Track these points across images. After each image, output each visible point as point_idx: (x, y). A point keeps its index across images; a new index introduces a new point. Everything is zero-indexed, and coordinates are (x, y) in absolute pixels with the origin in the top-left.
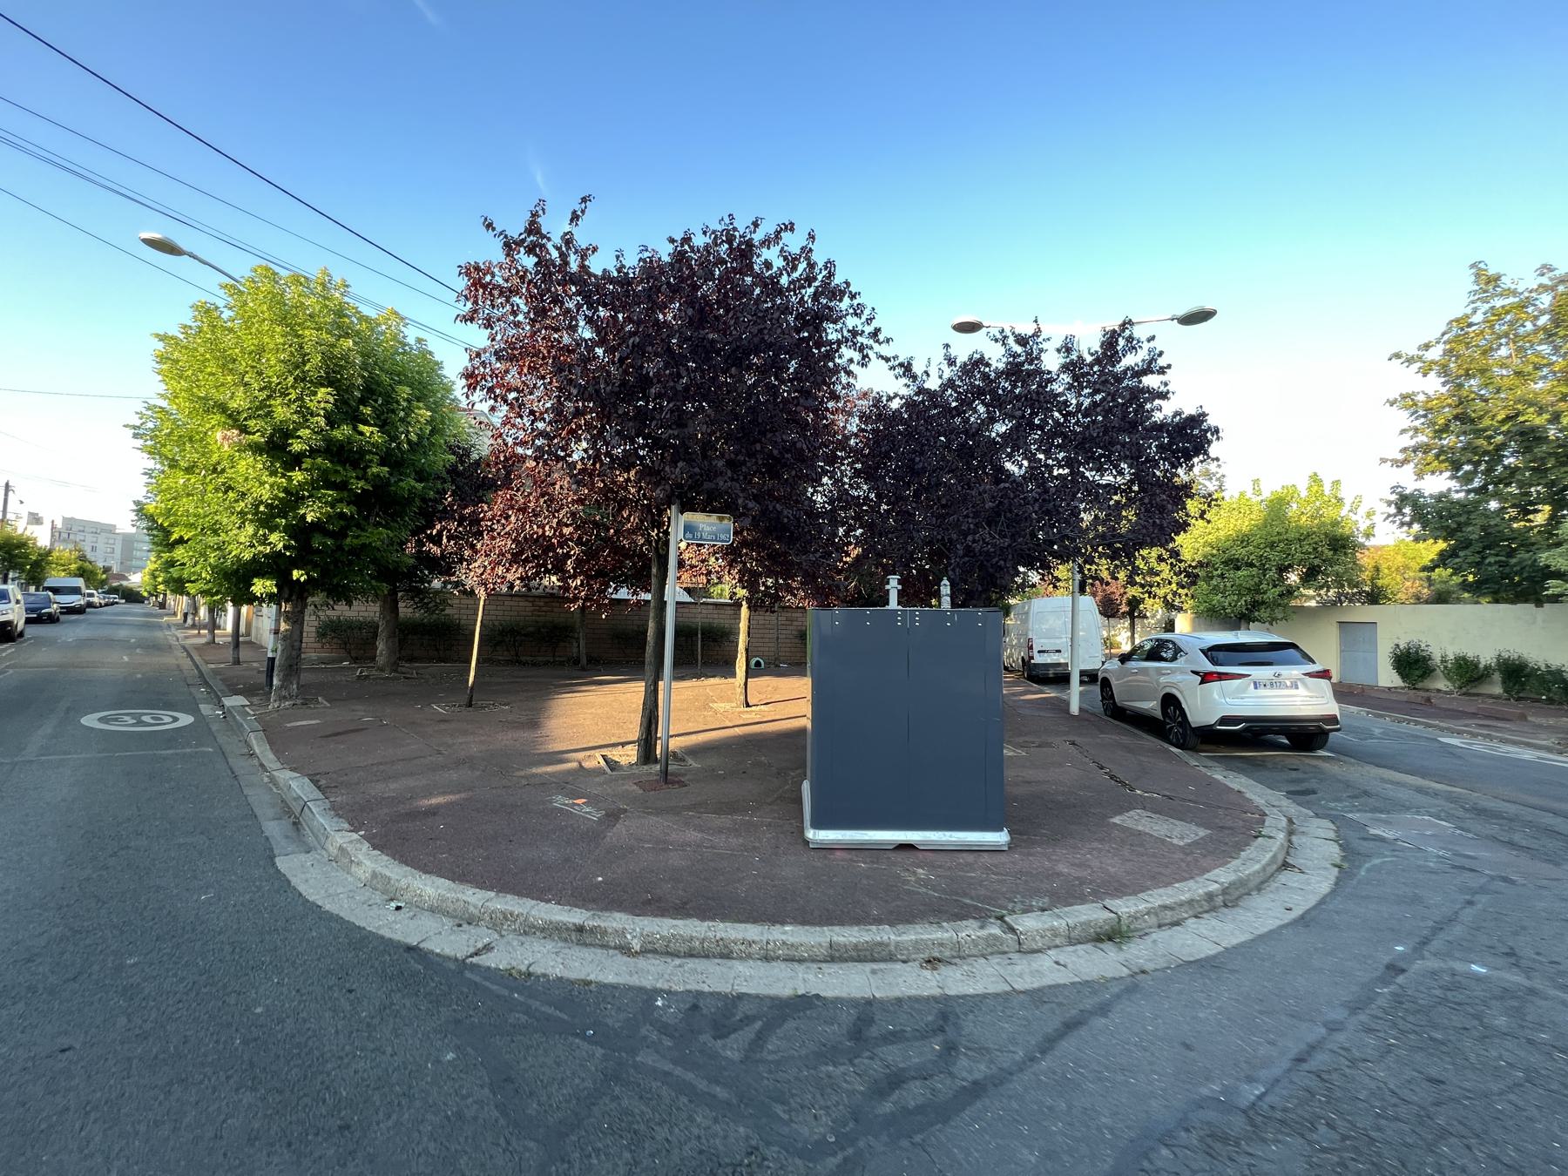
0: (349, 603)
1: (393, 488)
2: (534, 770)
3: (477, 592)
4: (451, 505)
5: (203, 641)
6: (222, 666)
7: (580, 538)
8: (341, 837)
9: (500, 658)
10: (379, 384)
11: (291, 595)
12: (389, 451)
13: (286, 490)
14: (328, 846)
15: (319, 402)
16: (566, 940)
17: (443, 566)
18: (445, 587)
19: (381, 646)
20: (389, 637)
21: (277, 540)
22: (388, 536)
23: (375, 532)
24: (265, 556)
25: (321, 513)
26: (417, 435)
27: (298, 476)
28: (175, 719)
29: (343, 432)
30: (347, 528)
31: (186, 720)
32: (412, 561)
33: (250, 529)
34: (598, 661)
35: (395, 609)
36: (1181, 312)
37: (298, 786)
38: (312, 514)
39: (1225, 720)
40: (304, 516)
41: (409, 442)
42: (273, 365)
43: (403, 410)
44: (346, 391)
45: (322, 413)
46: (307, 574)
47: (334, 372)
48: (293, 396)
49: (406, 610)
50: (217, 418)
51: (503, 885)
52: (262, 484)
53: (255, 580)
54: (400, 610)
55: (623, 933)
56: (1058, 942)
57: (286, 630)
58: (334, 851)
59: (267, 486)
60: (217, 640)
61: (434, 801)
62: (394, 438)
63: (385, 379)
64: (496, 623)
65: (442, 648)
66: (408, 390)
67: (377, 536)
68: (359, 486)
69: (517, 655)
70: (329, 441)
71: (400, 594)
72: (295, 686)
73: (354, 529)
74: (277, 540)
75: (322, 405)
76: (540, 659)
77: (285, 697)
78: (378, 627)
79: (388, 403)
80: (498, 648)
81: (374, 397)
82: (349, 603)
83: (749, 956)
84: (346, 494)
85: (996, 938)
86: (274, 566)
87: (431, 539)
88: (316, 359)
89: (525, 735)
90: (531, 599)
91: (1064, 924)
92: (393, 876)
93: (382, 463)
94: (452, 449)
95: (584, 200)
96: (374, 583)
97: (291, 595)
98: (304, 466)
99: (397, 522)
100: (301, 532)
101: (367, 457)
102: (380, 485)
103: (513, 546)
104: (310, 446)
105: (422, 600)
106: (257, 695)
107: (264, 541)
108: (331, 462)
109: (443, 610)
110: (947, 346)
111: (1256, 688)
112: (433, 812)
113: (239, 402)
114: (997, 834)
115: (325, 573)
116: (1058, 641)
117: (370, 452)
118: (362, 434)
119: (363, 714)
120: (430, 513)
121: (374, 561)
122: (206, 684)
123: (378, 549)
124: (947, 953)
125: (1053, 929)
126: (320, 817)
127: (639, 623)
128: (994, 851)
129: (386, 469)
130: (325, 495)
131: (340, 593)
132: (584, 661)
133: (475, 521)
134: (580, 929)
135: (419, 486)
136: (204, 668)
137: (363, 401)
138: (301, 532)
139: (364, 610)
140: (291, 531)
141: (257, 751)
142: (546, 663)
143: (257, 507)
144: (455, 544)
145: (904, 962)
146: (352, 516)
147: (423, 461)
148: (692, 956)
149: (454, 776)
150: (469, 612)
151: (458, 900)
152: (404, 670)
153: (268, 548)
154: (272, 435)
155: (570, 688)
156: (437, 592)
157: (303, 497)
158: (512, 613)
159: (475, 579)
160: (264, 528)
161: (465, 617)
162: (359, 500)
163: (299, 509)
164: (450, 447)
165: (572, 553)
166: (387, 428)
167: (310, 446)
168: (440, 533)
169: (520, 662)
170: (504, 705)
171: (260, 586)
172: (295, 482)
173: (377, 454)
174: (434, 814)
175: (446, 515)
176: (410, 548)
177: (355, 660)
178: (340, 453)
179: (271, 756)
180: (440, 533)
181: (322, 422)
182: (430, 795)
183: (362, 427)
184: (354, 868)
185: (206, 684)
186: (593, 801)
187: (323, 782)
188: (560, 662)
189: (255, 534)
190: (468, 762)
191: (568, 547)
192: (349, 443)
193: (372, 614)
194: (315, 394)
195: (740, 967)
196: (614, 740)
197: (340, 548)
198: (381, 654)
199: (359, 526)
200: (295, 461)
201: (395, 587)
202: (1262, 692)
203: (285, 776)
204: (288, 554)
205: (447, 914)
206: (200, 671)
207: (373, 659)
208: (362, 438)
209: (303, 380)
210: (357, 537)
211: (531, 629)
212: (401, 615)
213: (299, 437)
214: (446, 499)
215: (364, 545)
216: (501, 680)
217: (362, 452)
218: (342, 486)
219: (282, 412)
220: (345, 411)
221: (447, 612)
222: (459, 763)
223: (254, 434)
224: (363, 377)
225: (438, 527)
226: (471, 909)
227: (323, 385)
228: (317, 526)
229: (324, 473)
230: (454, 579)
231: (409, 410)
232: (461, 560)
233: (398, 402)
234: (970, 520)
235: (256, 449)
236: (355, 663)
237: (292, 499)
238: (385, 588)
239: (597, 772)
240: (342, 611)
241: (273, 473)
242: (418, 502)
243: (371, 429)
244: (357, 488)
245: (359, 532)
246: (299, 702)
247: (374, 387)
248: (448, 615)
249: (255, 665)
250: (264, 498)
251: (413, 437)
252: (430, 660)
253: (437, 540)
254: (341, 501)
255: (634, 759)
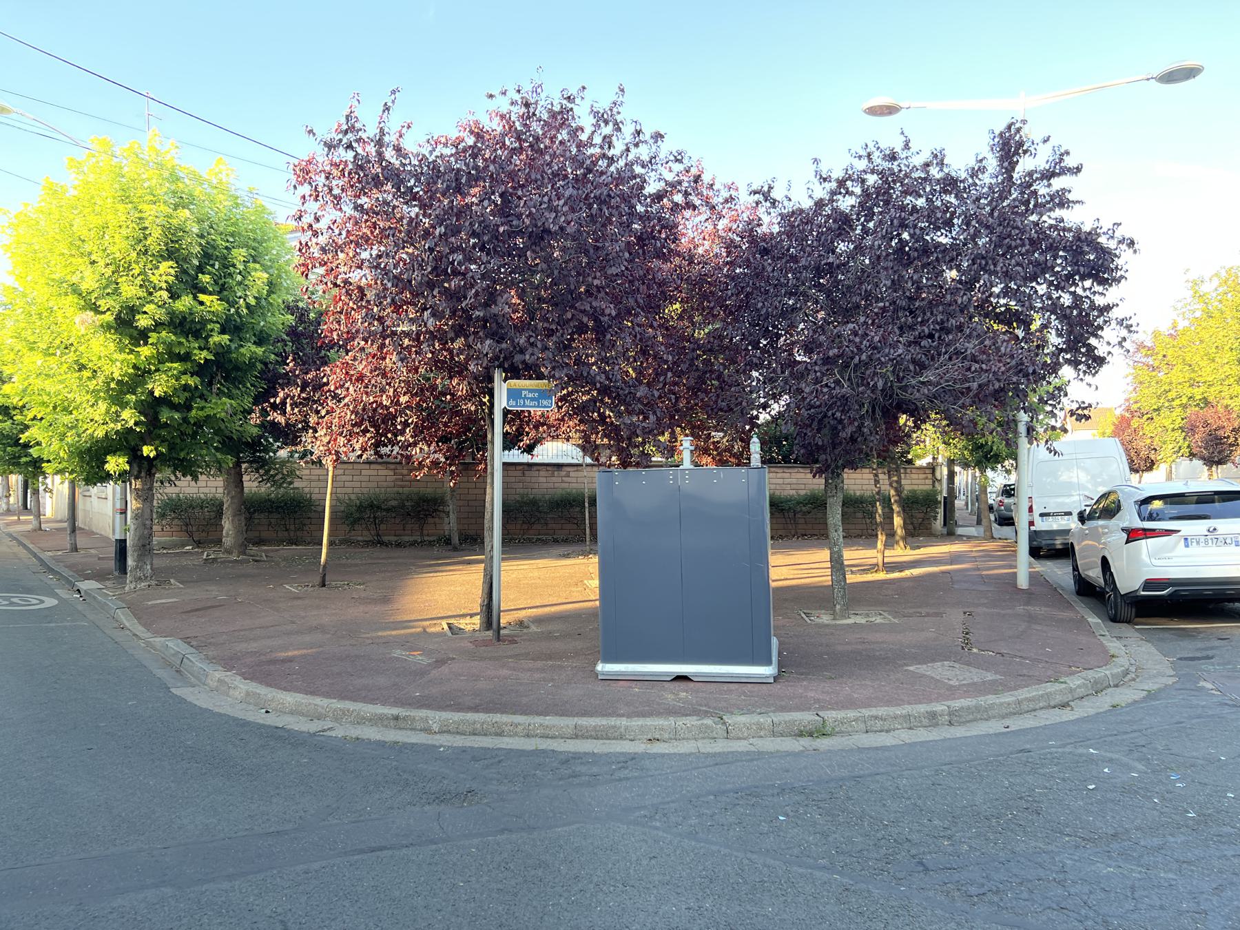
0: (195, 478)
1: (234, 355)
2: (380, 634)
3: (324, 462)
4: (293, 371)
5: (30, 527)
6: (60, 553)
7: (418, 404)
8: (217, 674)
9: (360, 538)
10: (214, 248)
11: (140, 472)
12: (229, 319)
13: (135, 367)
14: (209, 681)
15: (161, 275)
16: (386, 726)
17: (289, 435)
18: (292, 456)
19: (227, 524)
20: (234, 516)
21: (129, 417)
22: (231, 405)
23: (219, 402)
24: (117, 432)
25: (167, 387)
26: (256, 298)
27: (146, 351)
28: (42, 602)
29: (185, 303)
30: (192, 399)
31: (50, 602)
32: (255, 431)
33: (103, 406)
34: (476, 540)
35: (240, 483)
36: (1159, 69)
37: (175, 645)
38: (160, 388)
39: (1149, 584)
40: (151, 392)
41: (248, 306)
42: (119, 246)
43: (240, 273)
44: (185, 260)
45: (164, 285)
46: (156, 449)
47: (172, 241)
48: (136, 272)
49: (252, 484)
50: (72, 298)
51: (342, 696)
52: (113, 362)
53: (109, 458)
54: (246, 484)
55: (426, 720)
56: (762, 734)
57: (138, 509)
58: (214, 684)
59: (118, 364)
60: (43, 526)
61: (290, 654)
62: (232, 304)
63: (221, 243)
64: (353, 497)
65: (292, 527)
66: (243, 251)
67: (221, 406)
68: (202, 356)
69: (378, 535)
70: (172, 314)
71: (244, 466)
72: (149, 567)
73: (198, 400)
74: (129, 417)
75: (164, 278)
76: (406, 538)
77: (140, 578)
78: (222, 504)
79: (225, 266)
80: (356, 527)
81: (211, 262)
82: (195, 478)
83: (516, 734)
84: (189, 365)
85: (707, 727)
86: (126, 442)
87: (274, 407)
88: (156, 233)
89: (378, 608)
90: (392, 467)
91: (769, 720)
92: (262, 693)
93: (223, 332)
94: (290, 309)
95: (393, 92)
96: (219, 455)
97: (140, 472)
98: (150, 341)
99: (239, 389)
100: (151, 407)
101: (209, 327)
102: (222, 354)
103: (353, 417)
104: (155, 321)
105: (267, 472)
106: (109, 579)
107: (117, 418)
108: (175, 334)
109: (291, 483)
110: (816, 161)
111: (1187, 546)
112: (290, 660)
113: (89, 282)
114: (767, 668)
115: (172, 448)
116: (1067, 500)
117: (211, 321)
118: (202, 303)
119: (216, 592)
120: (271, 380)
121: (218, 432)
122: (51, 570)
123: (223, 420)
124: (666, 736)
125: (758, 723)
126: (196, 662)
127: (521, 491)
128: (760, 682)
129: (227, 337)
130: (170, 369)
131: (187, 468)
132: (455, 540)
133: (319, 386)
134: (396, 718)
135: (259, 351)
136: (43, 556)
137: (200, 269)
138: (151, 407)
139: (210, 486)
140: (142, 408)
141: (127, 624)
142: (413, 544)
143: (108, 384)
144: (300, 411)
145: (631, 740)
146: (196, 387)
147: (262, 324)
148: (475, 734)
149: (307, 638)
150: (476, 491)
151: (310, 704)
152: (252, 552)
153: (119, 424)
154: (120, 312)
155: (434, 568)
156: (283, 463)
157: (149, 372)
158: (370, 485)
159: (321, 448)
160: (116, 405)
161: (317, 490)
162: (201, 370)
163: (146, 383)
164: (288, 307)
165: (410, 421)
166: (225, 293)
167: (155, 321)
168: (284, 403)
169: (382, 543)
170: (360, 584)
171: (115, 464)
172: (142, 357)
173: (218, 322)
174: (291, 661)
175: (288, 380)
176: (255, 418)
177: (198, 544)
178: (184, 325)
179: (141, 628)
180: (284, 403)
181: (165, 295)
182: (287, 650)
183: (202, 297)
184: (231, 692)
185: (51, 570)
186: (427, 652)
187: (194, 643)
188: (430, 542)
189: (107, 412)
190: (321, 629)
191: (406, 415)
192: (191, 314)
193: (213, 490)
194: (157, 268)
195: (506, 739)
196: (463, 611)
197: (185, 420)
198: (227, 534)
199: (202, 397)
200: (142, 336)
201: (239, 458)
202: (1194, 549)
203: (158, 641)
204: (138, 430)
205: (303, 715)
206: (40, 560)
207: (219, 542)
208: (202, 308)
209: (146, 253)
210: (202, 409)
211: (394, 503)
212: (246, 490)
213: (145, 313)
214: (288, 365)
215: (208, 417)
216: (358, 562)
217: (204, 322)
218: (185, 358)
219: (130, 291)
220: (187, 283)
221: (296, 484)
222: (312, 629)
223: (104, 313)
224: (201, 245)
225: (281, 394)
226: (320, 709)
227: (165, 259)
228: (164, 401)
229: (169, 346)
230: (300, 448)
231: (245, 274)
232: (306, 427)
233: (234, 266)
234: (817, 368)
235: (107, 327)
236: (199, 547)
237: (141, 374)
238: (230, 460)
239: (441, 634)
240: (185, 487)
241: (121, 350)
242: (259, 366)
243: (211, 298)
244: (200, 358)
245: (203, 403)
246: (153, 583)
247: (210, 251)
248: (298, 488)
249: (92, 551)
250: (116, 375)
251: (252, 302)
252: (280, 542)
253: (281, 407)
254: (184, 373)
255: (477, 627)
